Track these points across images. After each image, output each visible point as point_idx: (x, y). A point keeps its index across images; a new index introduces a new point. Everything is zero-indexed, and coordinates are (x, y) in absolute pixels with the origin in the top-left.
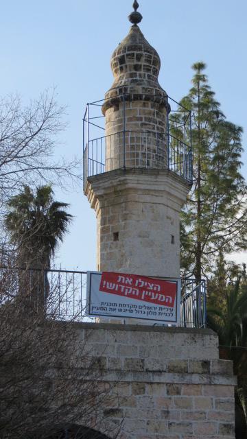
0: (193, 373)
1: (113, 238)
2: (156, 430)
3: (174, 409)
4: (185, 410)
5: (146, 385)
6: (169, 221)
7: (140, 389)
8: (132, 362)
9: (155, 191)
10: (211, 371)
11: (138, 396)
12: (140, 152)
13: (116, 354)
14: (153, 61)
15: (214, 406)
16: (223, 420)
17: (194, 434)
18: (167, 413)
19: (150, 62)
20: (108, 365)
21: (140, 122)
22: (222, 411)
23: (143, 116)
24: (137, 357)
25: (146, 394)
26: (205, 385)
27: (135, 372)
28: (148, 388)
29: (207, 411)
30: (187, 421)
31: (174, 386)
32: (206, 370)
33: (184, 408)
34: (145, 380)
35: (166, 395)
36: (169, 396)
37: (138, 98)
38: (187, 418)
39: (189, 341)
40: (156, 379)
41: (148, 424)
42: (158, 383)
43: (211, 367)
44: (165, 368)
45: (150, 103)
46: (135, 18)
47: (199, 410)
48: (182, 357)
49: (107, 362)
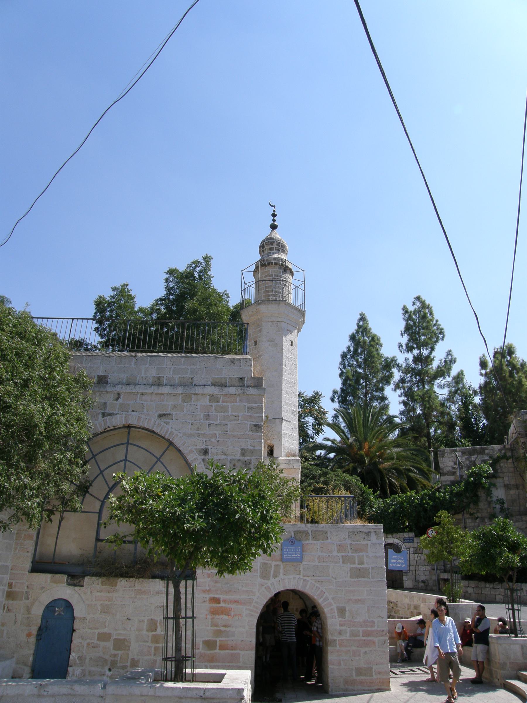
3: (214, 413)
5: (193, 396)
7: (187, 398)
11: (185, 404)
12: (271, 294)
13: (172, 374)
14: (375, 341)
15: (246, 411)
18: (207, 417)
19: (279, 246)
21: (271, 277)
24: (189, 376)
33: (222, 412)
35: (208, 403)
38: (224, 420)
40: (199, 390)
41: (192, 424)
44: (209, 383)
47: (233, 414)
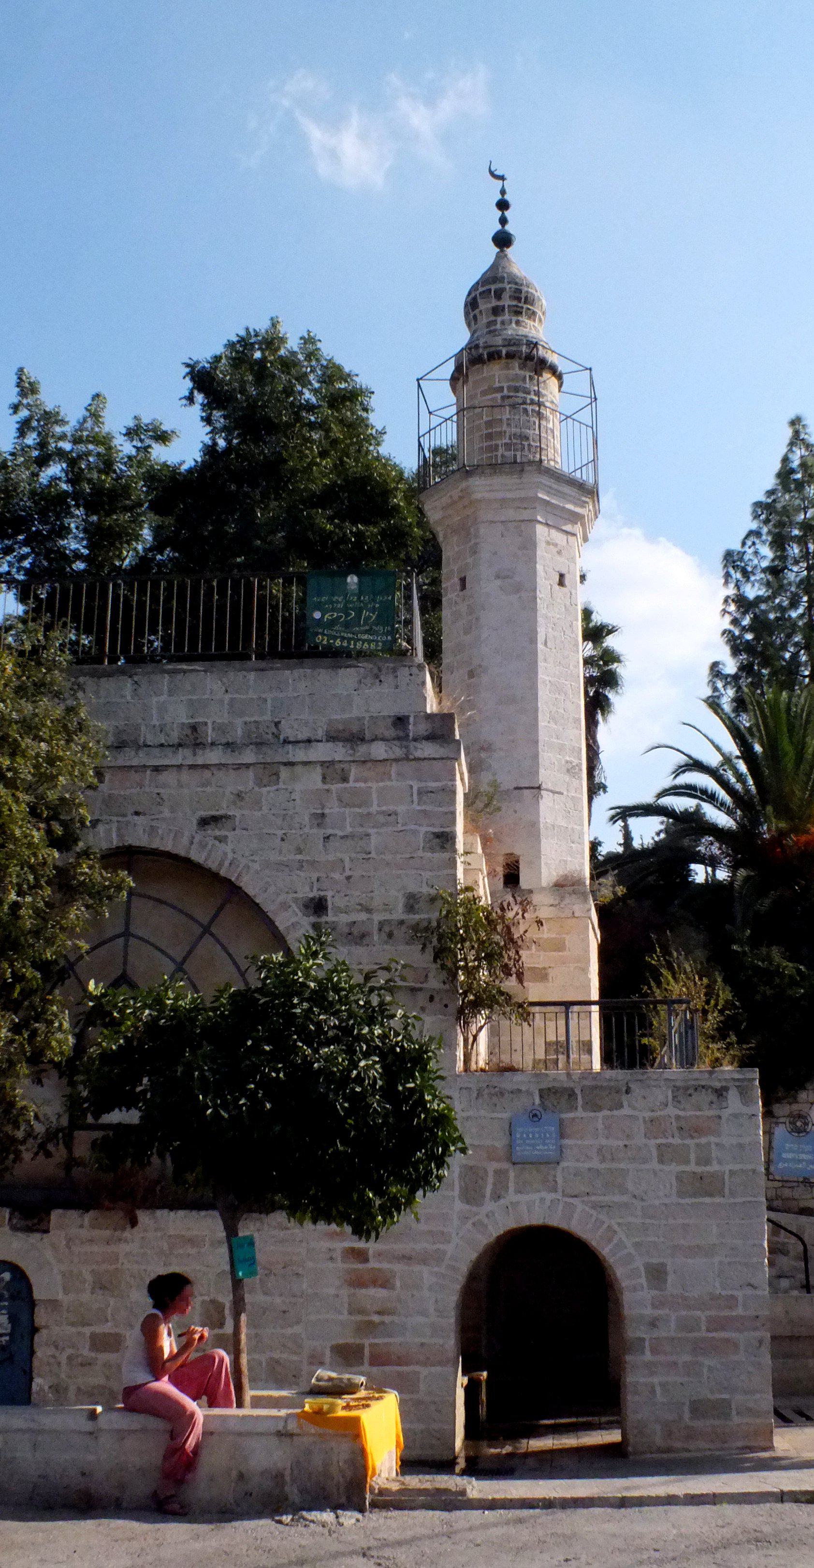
0: (373, 740)
1: (458, 588)
2: (299, 851)
4: (357, 810)
5: (282, 768)
6: (554, 550)
7: (270, 773)
8: (257, 728)
9: (522, 500)
10: (411, 735)
11: (264, 790)
16: (433, 825)
17: (373, 855)
18: (320, 818)
20: (210, 735)
21: (499, 395)
22: (428, 808)
23: (505, 385)
25: (281, 785)
26: (396, 760)
27: (260, 744)
28: (284, 773)
29: (401, 809)
30: (361, 830)
31: (337, 766)
32: (401, 734)
34: (279, 759)
36: (326, 787)
37: (494, 356)
38: (362, 826)
39: (369, 680)
40: (299, 754)
41: (283, 840)
42: (306, 763)
43: (411, 727)
44: (320, 734)
45: (516, 364)
46: (503, 240)
47: (384, 808)
48: (355, 713)
49: (210, 731)
